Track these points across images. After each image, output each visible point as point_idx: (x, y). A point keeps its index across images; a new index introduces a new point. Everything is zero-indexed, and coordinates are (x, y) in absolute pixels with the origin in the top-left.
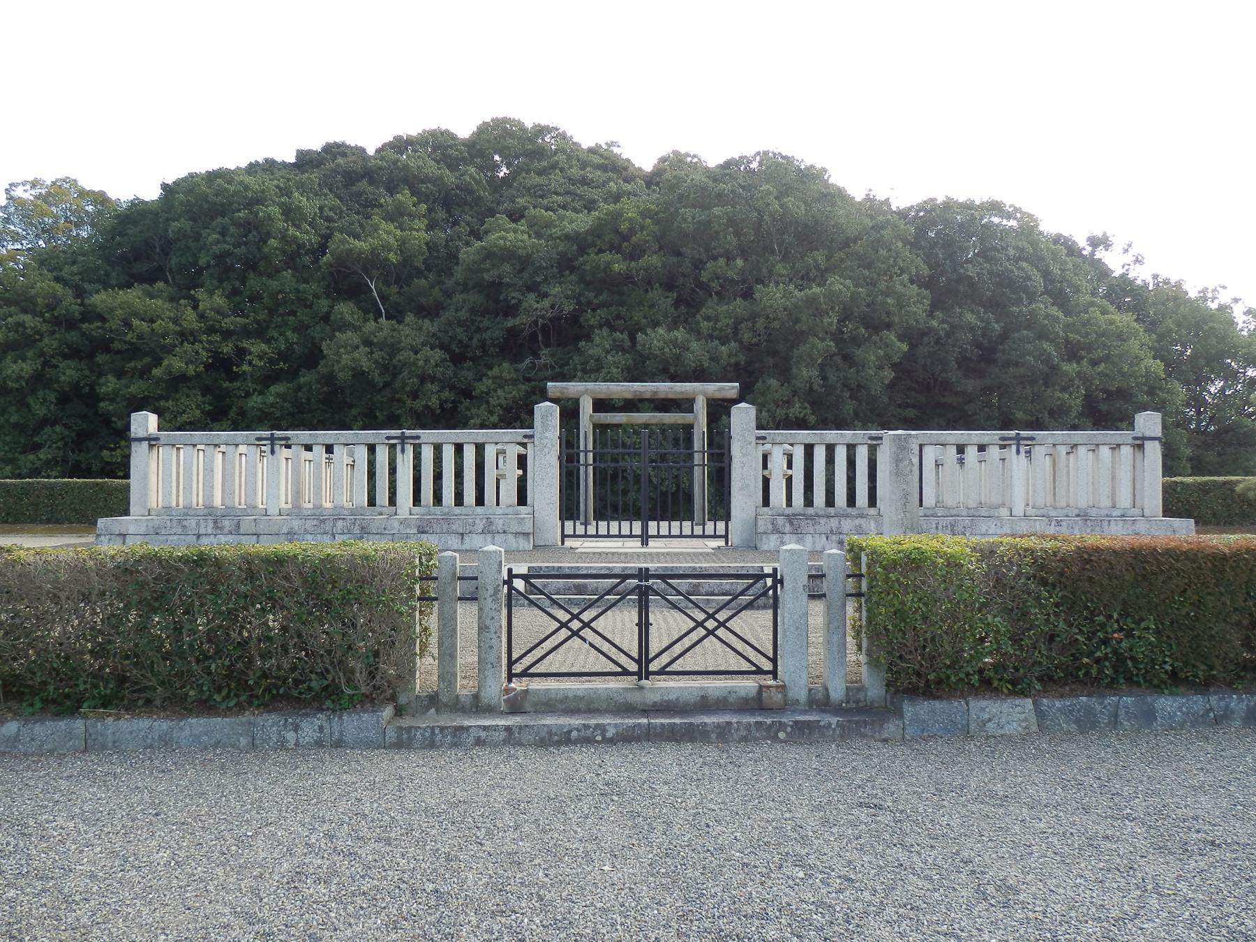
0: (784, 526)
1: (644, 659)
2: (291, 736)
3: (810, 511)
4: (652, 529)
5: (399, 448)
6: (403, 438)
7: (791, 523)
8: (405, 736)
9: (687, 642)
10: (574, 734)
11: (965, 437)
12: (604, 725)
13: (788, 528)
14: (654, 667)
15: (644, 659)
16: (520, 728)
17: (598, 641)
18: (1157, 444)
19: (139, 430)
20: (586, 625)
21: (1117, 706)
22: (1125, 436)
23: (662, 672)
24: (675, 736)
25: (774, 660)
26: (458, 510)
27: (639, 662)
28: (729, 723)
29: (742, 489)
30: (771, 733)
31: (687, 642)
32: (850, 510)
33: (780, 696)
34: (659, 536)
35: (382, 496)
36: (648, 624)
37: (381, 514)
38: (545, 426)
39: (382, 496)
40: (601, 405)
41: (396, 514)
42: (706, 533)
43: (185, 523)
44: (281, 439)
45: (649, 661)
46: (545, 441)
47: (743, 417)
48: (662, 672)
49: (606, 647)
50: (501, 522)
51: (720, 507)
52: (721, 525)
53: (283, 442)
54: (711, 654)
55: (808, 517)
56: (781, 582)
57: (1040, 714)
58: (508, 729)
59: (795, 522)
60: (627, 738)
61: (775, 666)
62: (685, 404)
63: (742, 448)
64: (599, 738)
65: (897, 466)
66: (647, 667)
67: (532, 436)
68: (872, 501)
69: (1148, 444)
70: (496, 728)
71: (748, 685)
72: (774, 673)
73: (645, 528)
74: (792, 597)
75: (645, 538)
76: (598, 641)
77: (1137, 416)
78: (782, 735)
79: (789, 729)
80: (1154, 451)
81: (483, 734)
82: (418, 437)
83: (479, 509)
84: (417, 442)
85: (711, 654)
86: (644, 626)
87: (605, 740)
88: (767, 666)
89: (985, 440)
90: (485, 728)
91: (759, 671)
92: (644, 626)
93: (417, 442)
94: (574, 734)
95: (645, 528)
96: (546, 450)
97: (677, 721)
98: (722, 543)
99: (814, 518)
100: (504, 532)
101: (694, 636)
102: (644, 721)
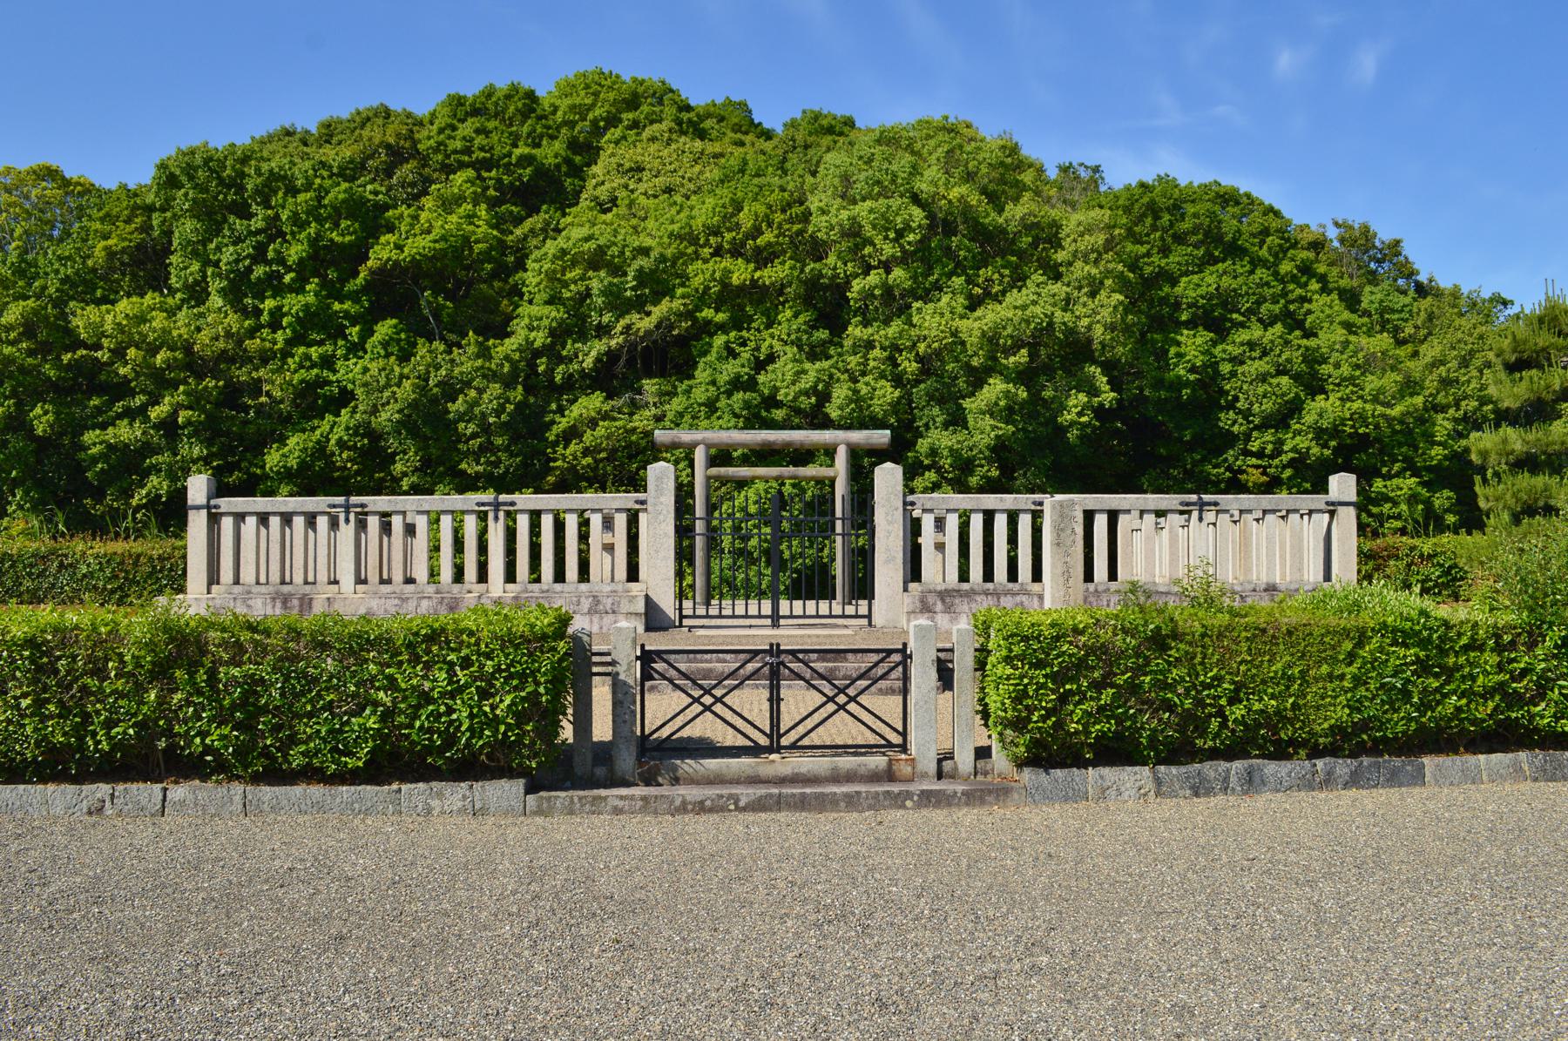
0: (935, 604)
1: (775, 732)
2: (435, 803)
3: (965, 586)
4: (784, 607)
5: (491, 516)
6: (497, 505)
7: (943, 601)
8: (545, 805)
9: (817, 718)
10: (708, 803)
11: (1141, 501)
12: (737, 795)
13: (939, 606)
14: (785, 741)
15: (775, 732)
16: (656, 797)
17: (728, 715)
18: (1352, 511)
19: (197, 495)
20: (718, 700)
21: (1228, 771)
22: (1318, 501)
23: (794, 746)
24: (802, 804)
25: (904, 734)
26: (558, 587)
27: (770, 736)
28: (858, 793)
29: (887, 561)
30: (898, 801)
31: (817, 718)
32: (1011, 585)
33: (909, 769)
34: (791, 617)
35: (471, 572)
36: (779, 700)
37: (469, 592)
38: (659, 489)
39: (471, 572)
40: (720, 457)
41: (487, 591)
42: (724, 613)
43: (249, 602)
44: (356, 506)
45: (780, 736)
46: (659, 508)
47: (887, 477)
48: (794, 746)
49: (739, 723)
50: (610, 601)
51: (863, 588)
52: (863, 603)
53: (359, 510)
54: (842, 729)
55: (986, 593)
56: (911, 657)
57: (1158, 782)
58: (644, 799)
59: (948, 600)
60: (758, 806)
61: (905, 740)
62: (830, 452)
63: (887, 514)
64: (732, 807)
65: (1058, 535)
66: (778, 742)
67: (643, 502)
68: (1037, 576)
69: (1341, 509)
70: (632, 798)
71: (877, 762)
72: (904, 748)
73: (775, 608)
74: (923, 676)
75: (775, 618)
76: (728, 715)
77: (1331, 478)
78: (909, 803)
79: (916, 798)
80: (1348, 517)
81: (620, 804)
82: (513, 504)
83: (584, 587)
84: (511, 508)
85: (842, 729)
86: (775, 700)
87: (737, 809)
88: (896, 739)
89: (1163, 506)
90: (622, 798)
91: (890, 745)
92: (775, 700)
93: (511, 508)
94: (708, 803)
95: (775, 608)
96: (661, 517)
97: (808, 791)
98: (865, 622)
99: (971, 594)
100: (614, 612)
101: (823, 713)
102: (775, 791)
